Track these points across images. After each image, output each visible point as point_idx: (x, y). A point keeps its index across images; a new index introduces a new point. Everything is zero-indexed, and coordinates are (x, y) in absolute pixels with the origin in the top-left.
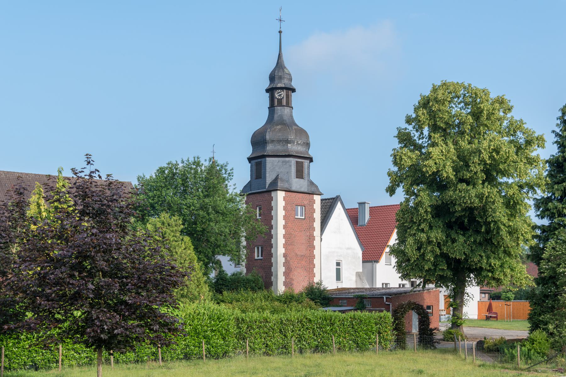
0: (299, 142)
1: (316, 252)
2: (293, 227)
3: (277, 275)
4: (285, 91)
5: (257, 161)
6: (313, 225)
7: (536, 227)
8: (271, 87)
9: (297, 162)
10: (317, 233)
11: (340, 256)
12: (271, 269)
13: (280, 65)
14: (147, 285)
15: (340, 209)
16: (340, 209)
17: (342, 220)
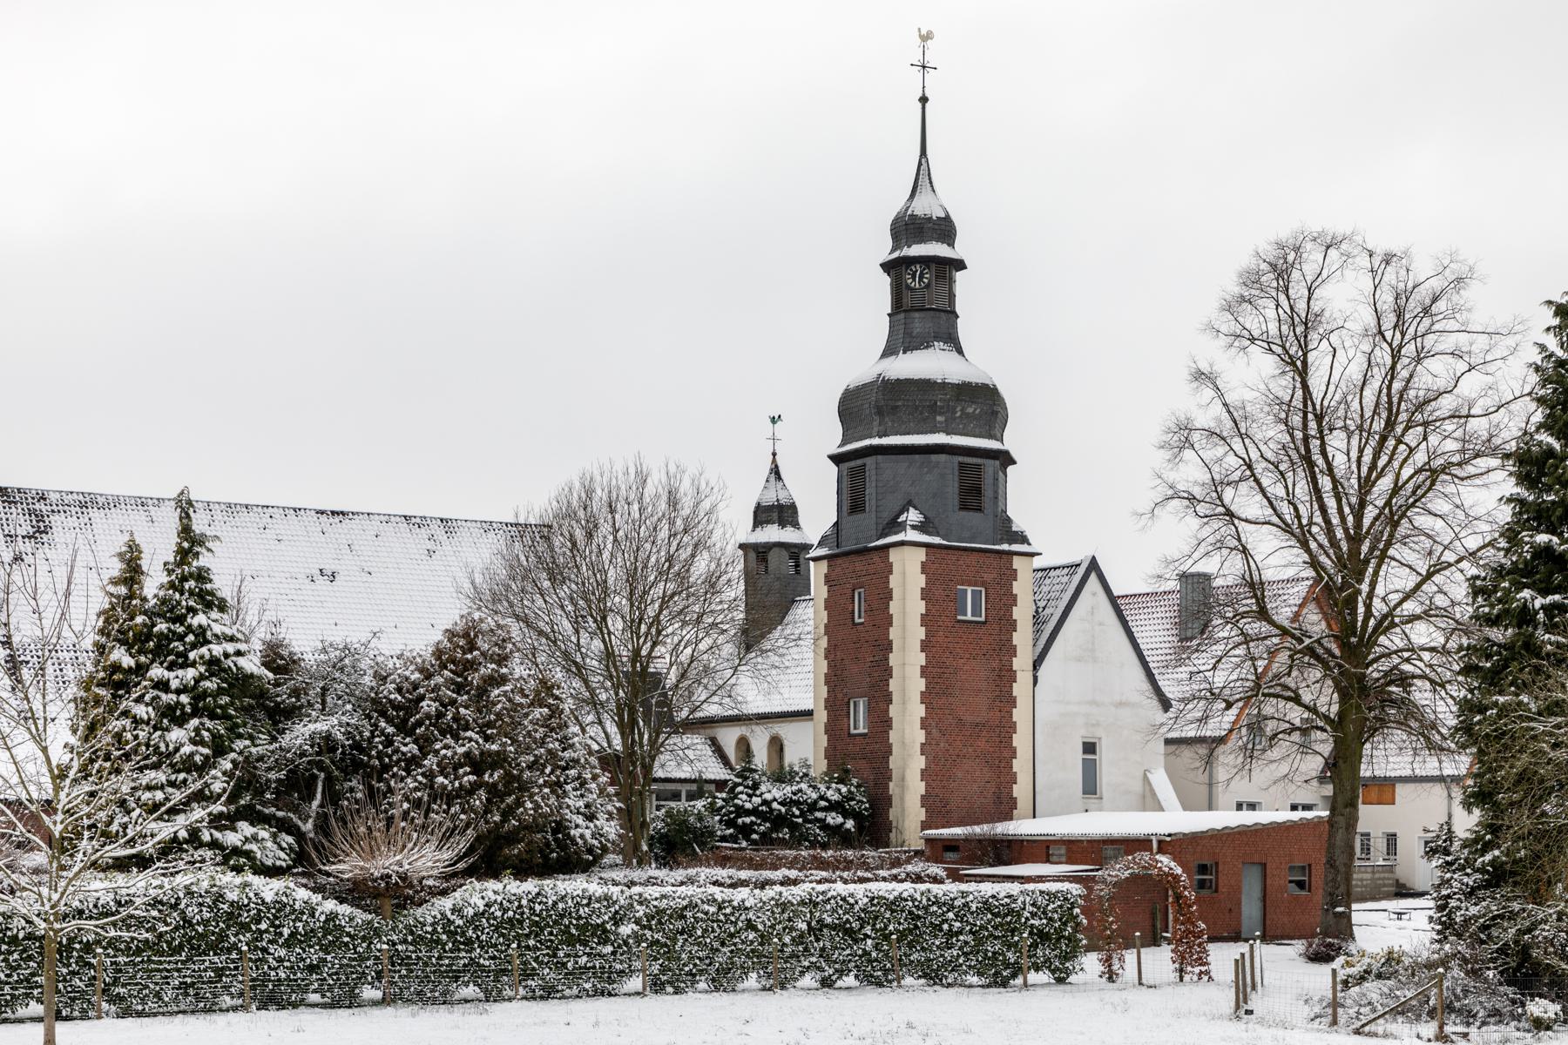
0: (970, 410)
1: (1020, 715)
2: (951, 645)
3: (903, 779)
4: (933, 266)
5: (852, 464)
8: (896, 255)
10: (1022, 662)
11: (1093, 725)
12: (888, 762)
15: (1094, 594)
17: (1101, 624)
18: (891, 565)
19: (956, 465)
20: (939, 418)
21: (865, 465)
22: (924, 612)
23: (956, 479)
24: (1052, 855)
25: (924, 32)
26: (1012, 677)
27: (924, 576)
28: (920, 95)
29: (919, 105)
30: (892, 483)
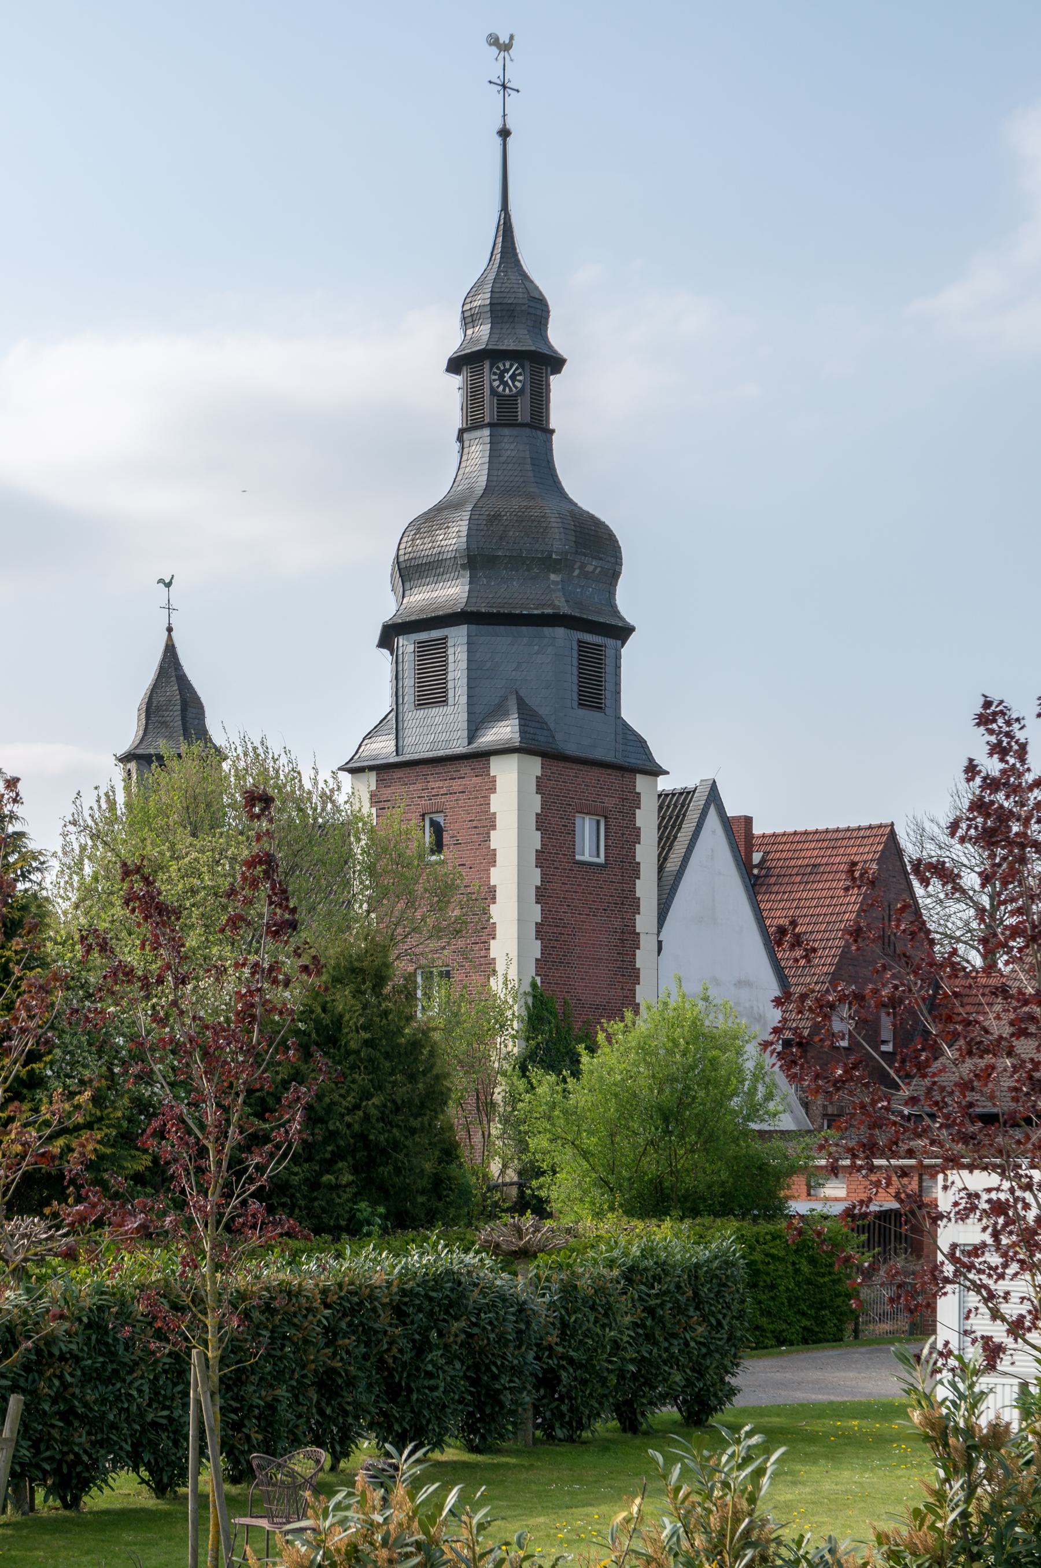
0: (590, 568)
5: (424, 636)
6: (633, 890)
10: (645, 921)
13: (170, 651)
14: (587, 1360)
16: (714, 832)
28: (499, 125)
29: (499, 141)
30: (488, 665)
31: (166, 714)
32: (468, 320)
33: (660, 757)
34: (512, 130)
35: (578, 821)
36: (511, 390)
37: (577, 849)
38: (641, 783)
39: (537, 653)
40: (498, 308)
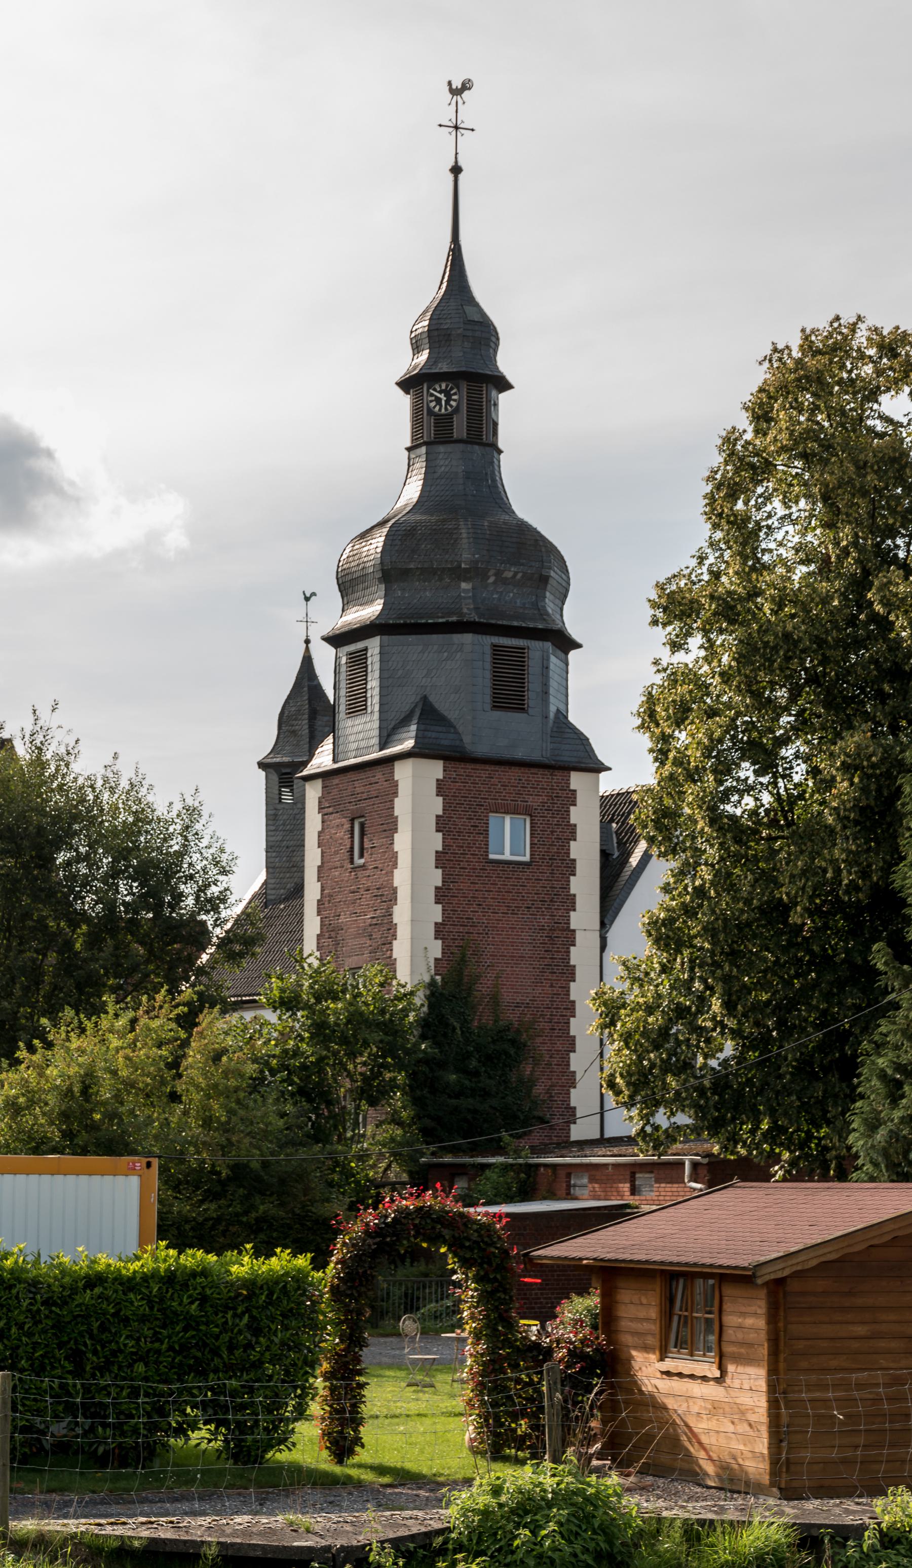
0: (508, 574)
4: (464, 386)
7: (34, 1545)
9: (495, 648)
18: (396, 785)
19: (488, 650)
20: (464, 585)
21: (366, 649)
22: (440, 848)
23: (488, 666)
24: (575, 1186)
25: (457, 84)
26: (569, 938)
27: (440, 799)
28: (451, 163)
29: (451, 177)
31: (295, 723)
32: (416, 348)
33: (602, 754)
34: (463, 167)
35: (493, 818)
36: (440, 410)
37: (492, 847)
38: (577, 780)
39: (447, 659)
40: (436, 333)
